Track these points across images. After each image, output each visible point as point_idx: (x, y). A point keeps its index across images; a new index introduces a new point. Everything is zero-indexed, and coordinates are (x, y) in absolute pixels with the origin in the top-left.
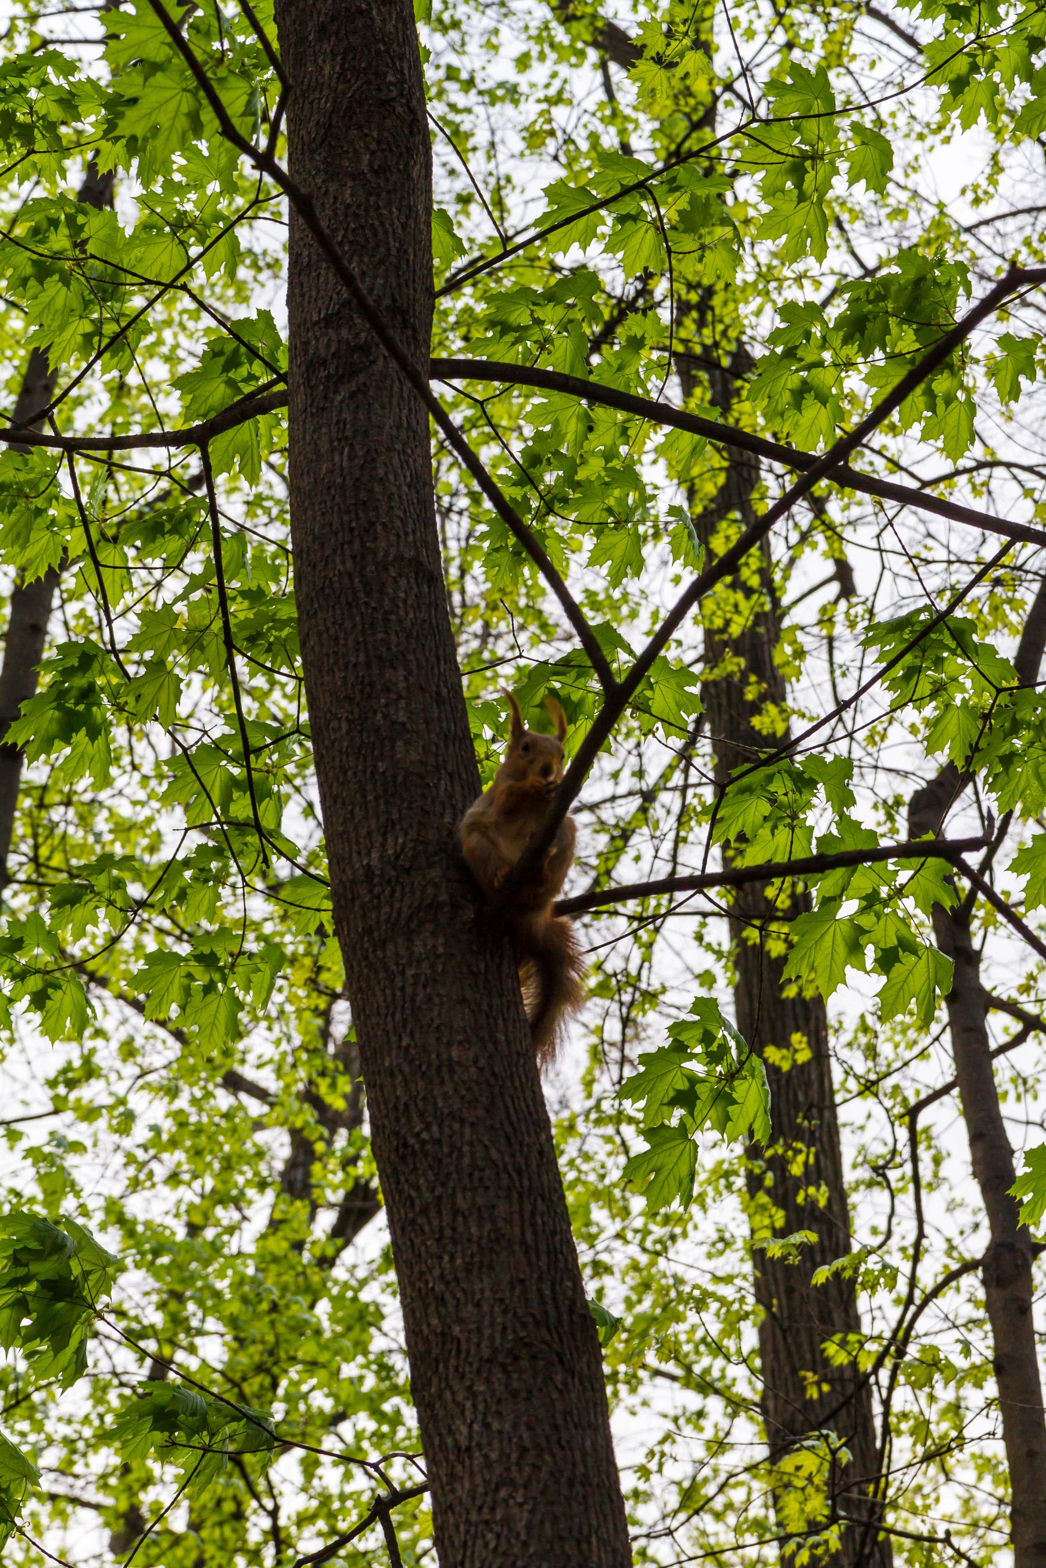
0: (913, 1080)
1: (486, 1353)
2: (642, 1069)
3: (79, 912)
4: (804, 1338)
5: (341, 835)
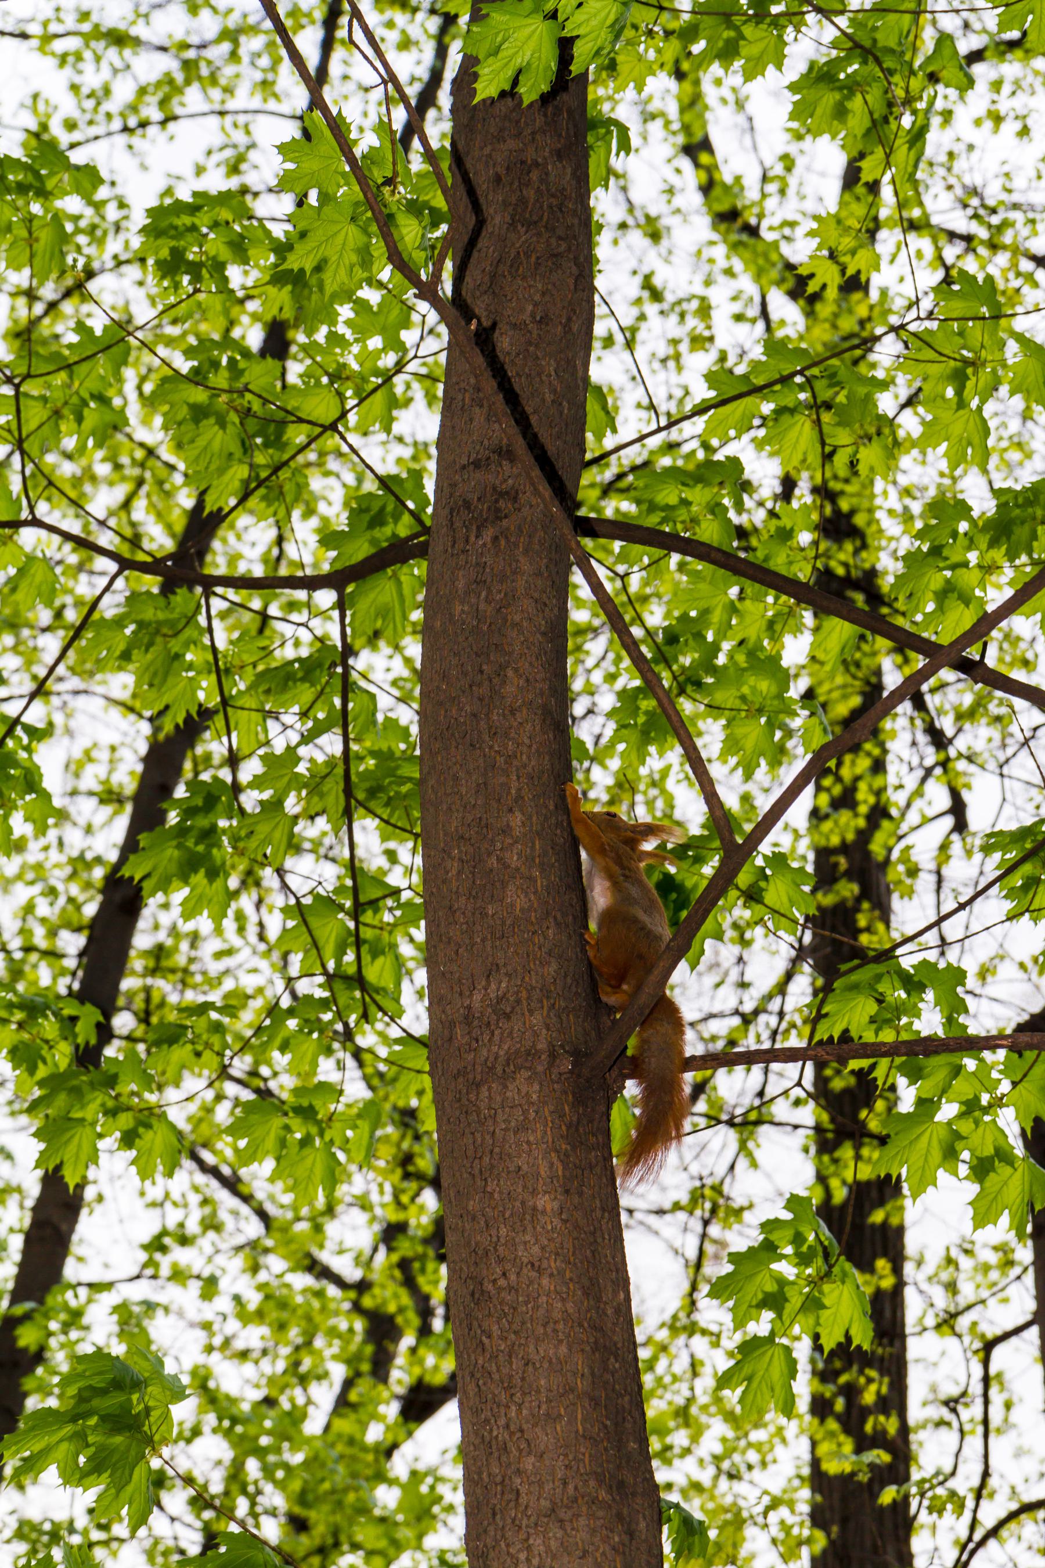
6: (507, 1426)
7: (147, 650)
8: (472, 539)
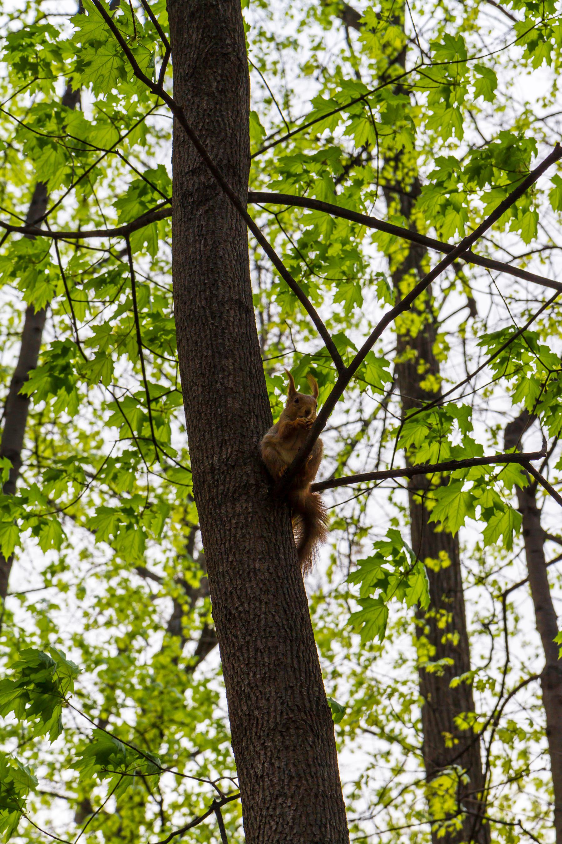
0: (504, 577)
1: (272, 726)
2: (360, 567)
3: (58, 484)
4: (445, 715)
5: (198, 448)
7: (25, 271)
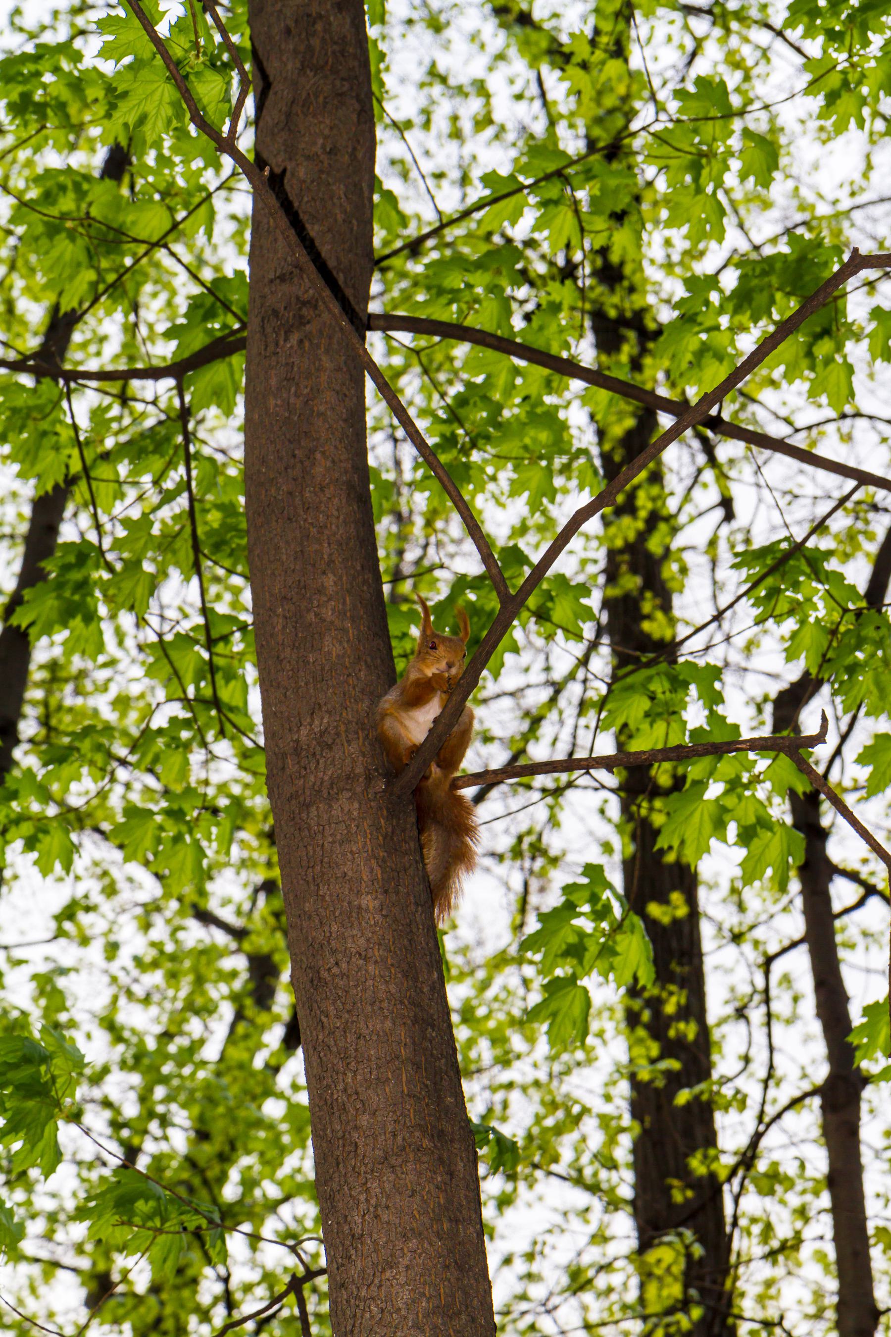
3: (67, 770)
6: (345, 1090)
8: (281, 342)
